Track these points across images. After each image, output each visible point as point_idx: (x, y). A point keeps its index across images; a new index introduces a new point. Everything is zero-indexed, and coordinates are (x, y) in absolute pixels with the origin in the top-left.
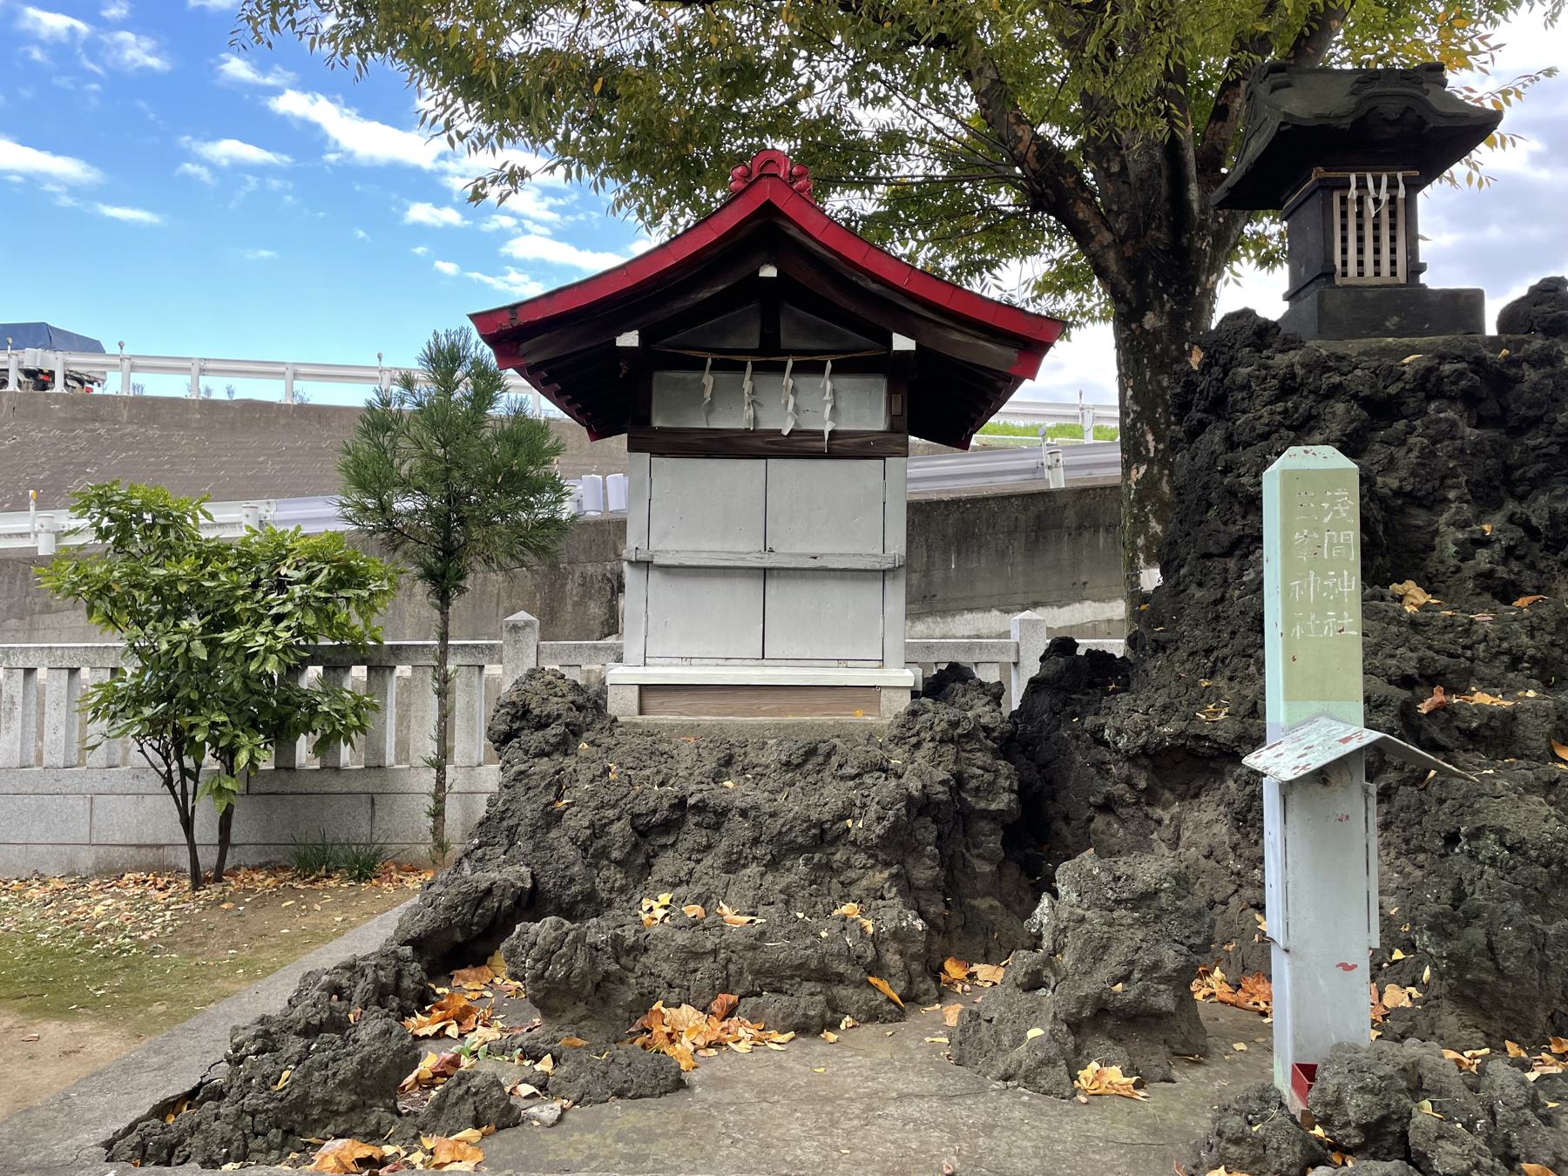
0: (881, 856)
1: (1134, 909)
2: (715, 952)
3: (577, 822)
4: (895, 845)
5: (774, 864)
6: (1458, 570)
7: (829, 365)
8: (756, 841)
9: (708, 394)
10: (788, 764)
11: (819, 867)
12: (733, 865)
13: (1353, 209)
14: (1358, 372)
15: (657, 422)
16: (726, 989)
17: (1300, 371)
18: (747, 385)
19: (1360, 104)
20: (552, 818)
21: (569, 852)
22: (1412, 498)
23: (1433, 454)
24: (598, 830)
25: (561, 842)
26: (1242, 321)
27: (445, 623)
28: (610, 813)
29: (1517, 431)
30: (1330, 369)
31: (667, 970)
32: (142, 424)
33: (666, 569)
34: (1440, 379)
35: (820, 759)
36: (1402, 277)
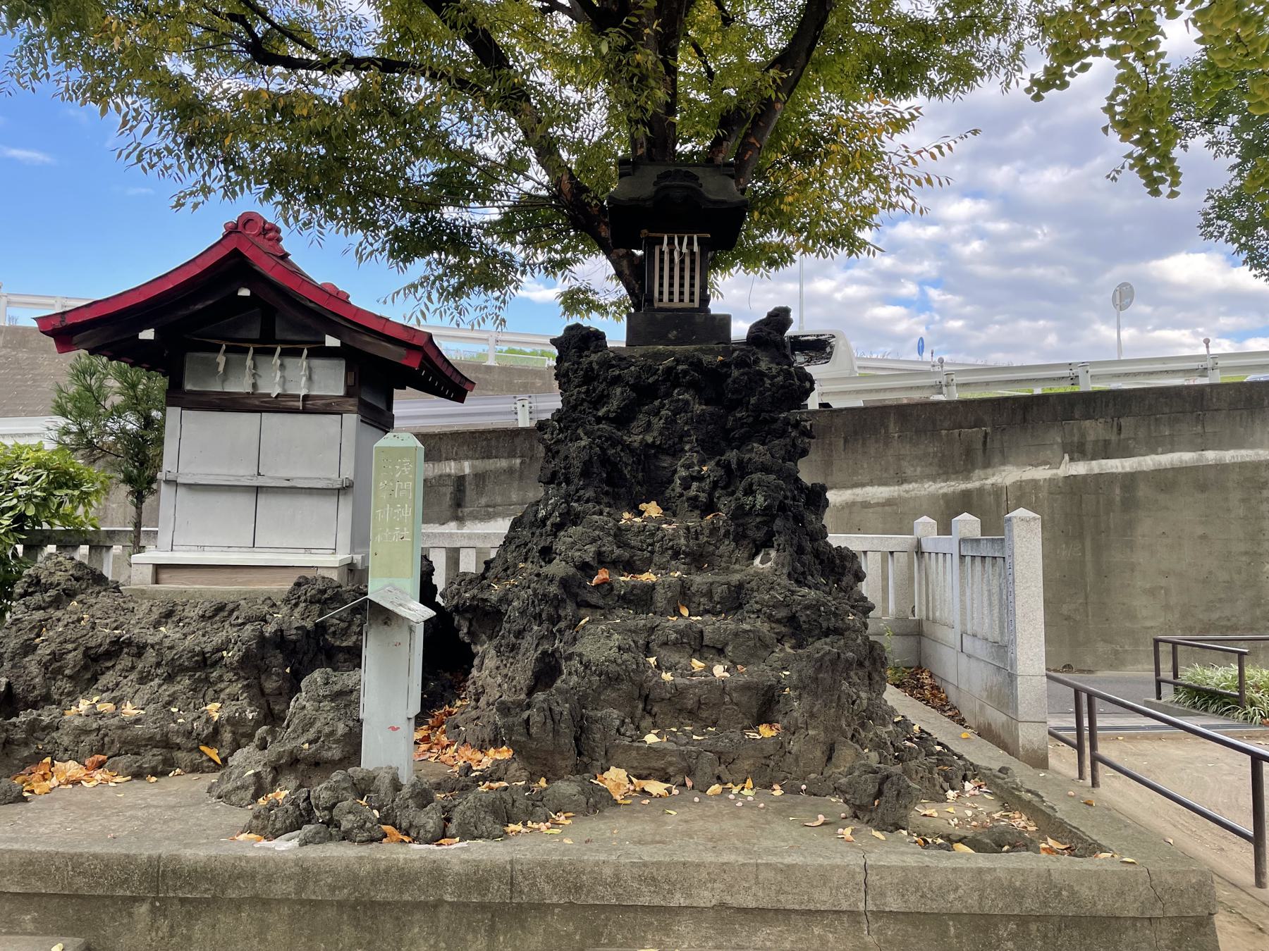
0: (242, 674)
1: (332, 701)
2: (99, 730)
3: (44, 651)
4: (252, 665)
5: (170, 679)
6: (681, 495)
7: (305, 352)
8: (158, 665)
9: (221, 369)
10: (203, 616)
11: (200, 680)
12: (143, 680)
13: (666, 258)
14: (633, 368)
15: (188, 387)
16: (100, 752)
17: (595, 366)
18: (249, 362)
19: (657, 192)
20: (28, 648)
21: (34, 669)
22: (660, 450)
23: (675, 421)
24: (56, 657)
25: (32, 665)
26: (574, 332)
27: (139, 515)
28: (70, 646)
29: (732, 406)
30: (613, 366)
31: (66, 741)
32: (14, 348)
33: (190, 487)
34: (677, 374)
35: (226, 614)
36: (696, 304)
